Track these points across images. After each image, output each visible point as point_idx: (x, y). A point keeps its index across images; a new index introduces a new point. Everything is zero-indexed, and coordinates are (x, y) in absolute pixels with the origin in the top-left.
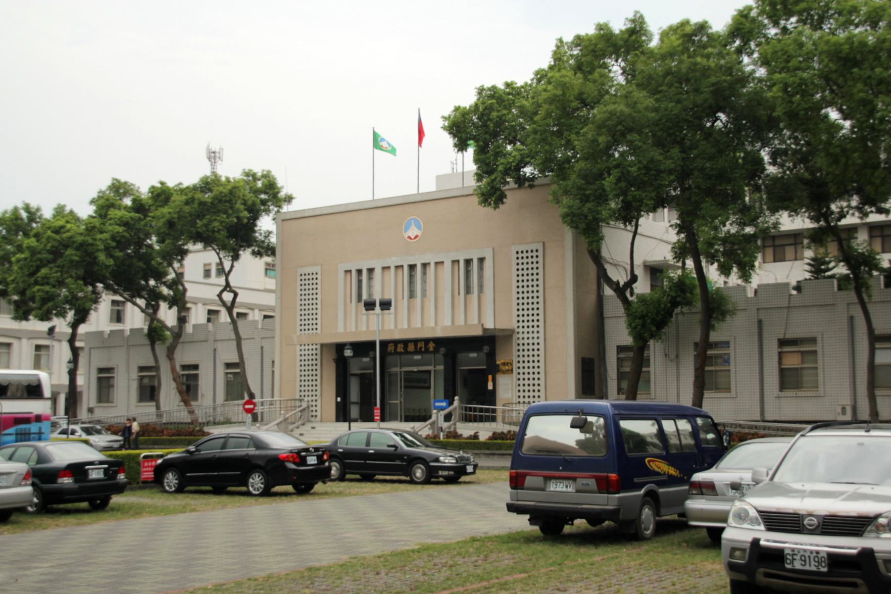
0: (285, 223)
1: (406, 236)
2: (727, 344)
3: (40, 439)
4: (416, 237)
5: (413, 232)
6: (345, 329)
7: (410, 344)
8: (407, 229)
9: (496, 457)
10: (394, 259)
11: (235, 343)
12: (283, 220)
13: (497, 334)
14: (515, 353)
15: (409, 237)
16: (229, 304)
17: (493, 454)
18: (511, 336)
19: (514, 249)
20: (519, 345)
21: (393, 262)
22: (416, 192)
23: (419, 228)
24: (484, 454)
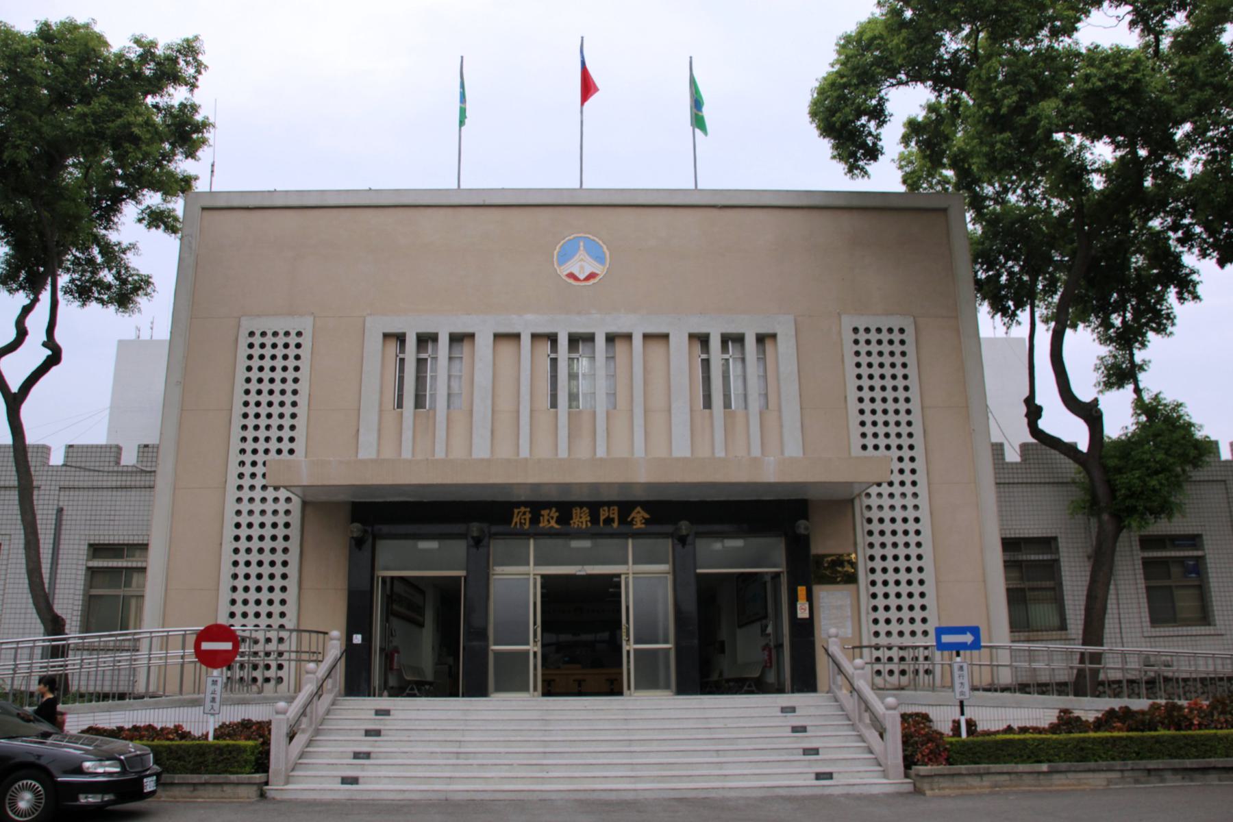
0: (206, 213)
1: (564, 270)
2: (1194, 540)
3: (1082, 654)
4: (592, 276)
5: (582, 265)
6: (447, 455)
7: (576, 511)
8: (565, 257)
9: (1212, 778)
10: (530, 317)
11: (14, 496)
12: (204, 209)
13: (811, 495)
14: (862, 540)
15: (572, 276)
16: (14, 387)
17: (1204, 770)
18: (852, 501)
19: (848, 323)
20: (870, 521)
21: (527, 324)
22: (578, 186)
23: (600, 259)
24: (1175, 771)
